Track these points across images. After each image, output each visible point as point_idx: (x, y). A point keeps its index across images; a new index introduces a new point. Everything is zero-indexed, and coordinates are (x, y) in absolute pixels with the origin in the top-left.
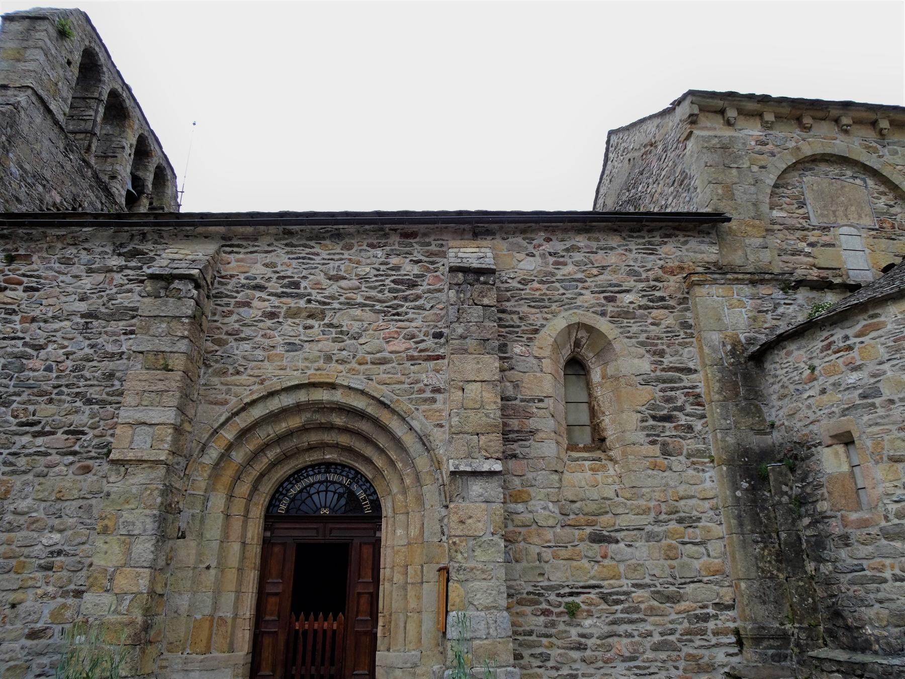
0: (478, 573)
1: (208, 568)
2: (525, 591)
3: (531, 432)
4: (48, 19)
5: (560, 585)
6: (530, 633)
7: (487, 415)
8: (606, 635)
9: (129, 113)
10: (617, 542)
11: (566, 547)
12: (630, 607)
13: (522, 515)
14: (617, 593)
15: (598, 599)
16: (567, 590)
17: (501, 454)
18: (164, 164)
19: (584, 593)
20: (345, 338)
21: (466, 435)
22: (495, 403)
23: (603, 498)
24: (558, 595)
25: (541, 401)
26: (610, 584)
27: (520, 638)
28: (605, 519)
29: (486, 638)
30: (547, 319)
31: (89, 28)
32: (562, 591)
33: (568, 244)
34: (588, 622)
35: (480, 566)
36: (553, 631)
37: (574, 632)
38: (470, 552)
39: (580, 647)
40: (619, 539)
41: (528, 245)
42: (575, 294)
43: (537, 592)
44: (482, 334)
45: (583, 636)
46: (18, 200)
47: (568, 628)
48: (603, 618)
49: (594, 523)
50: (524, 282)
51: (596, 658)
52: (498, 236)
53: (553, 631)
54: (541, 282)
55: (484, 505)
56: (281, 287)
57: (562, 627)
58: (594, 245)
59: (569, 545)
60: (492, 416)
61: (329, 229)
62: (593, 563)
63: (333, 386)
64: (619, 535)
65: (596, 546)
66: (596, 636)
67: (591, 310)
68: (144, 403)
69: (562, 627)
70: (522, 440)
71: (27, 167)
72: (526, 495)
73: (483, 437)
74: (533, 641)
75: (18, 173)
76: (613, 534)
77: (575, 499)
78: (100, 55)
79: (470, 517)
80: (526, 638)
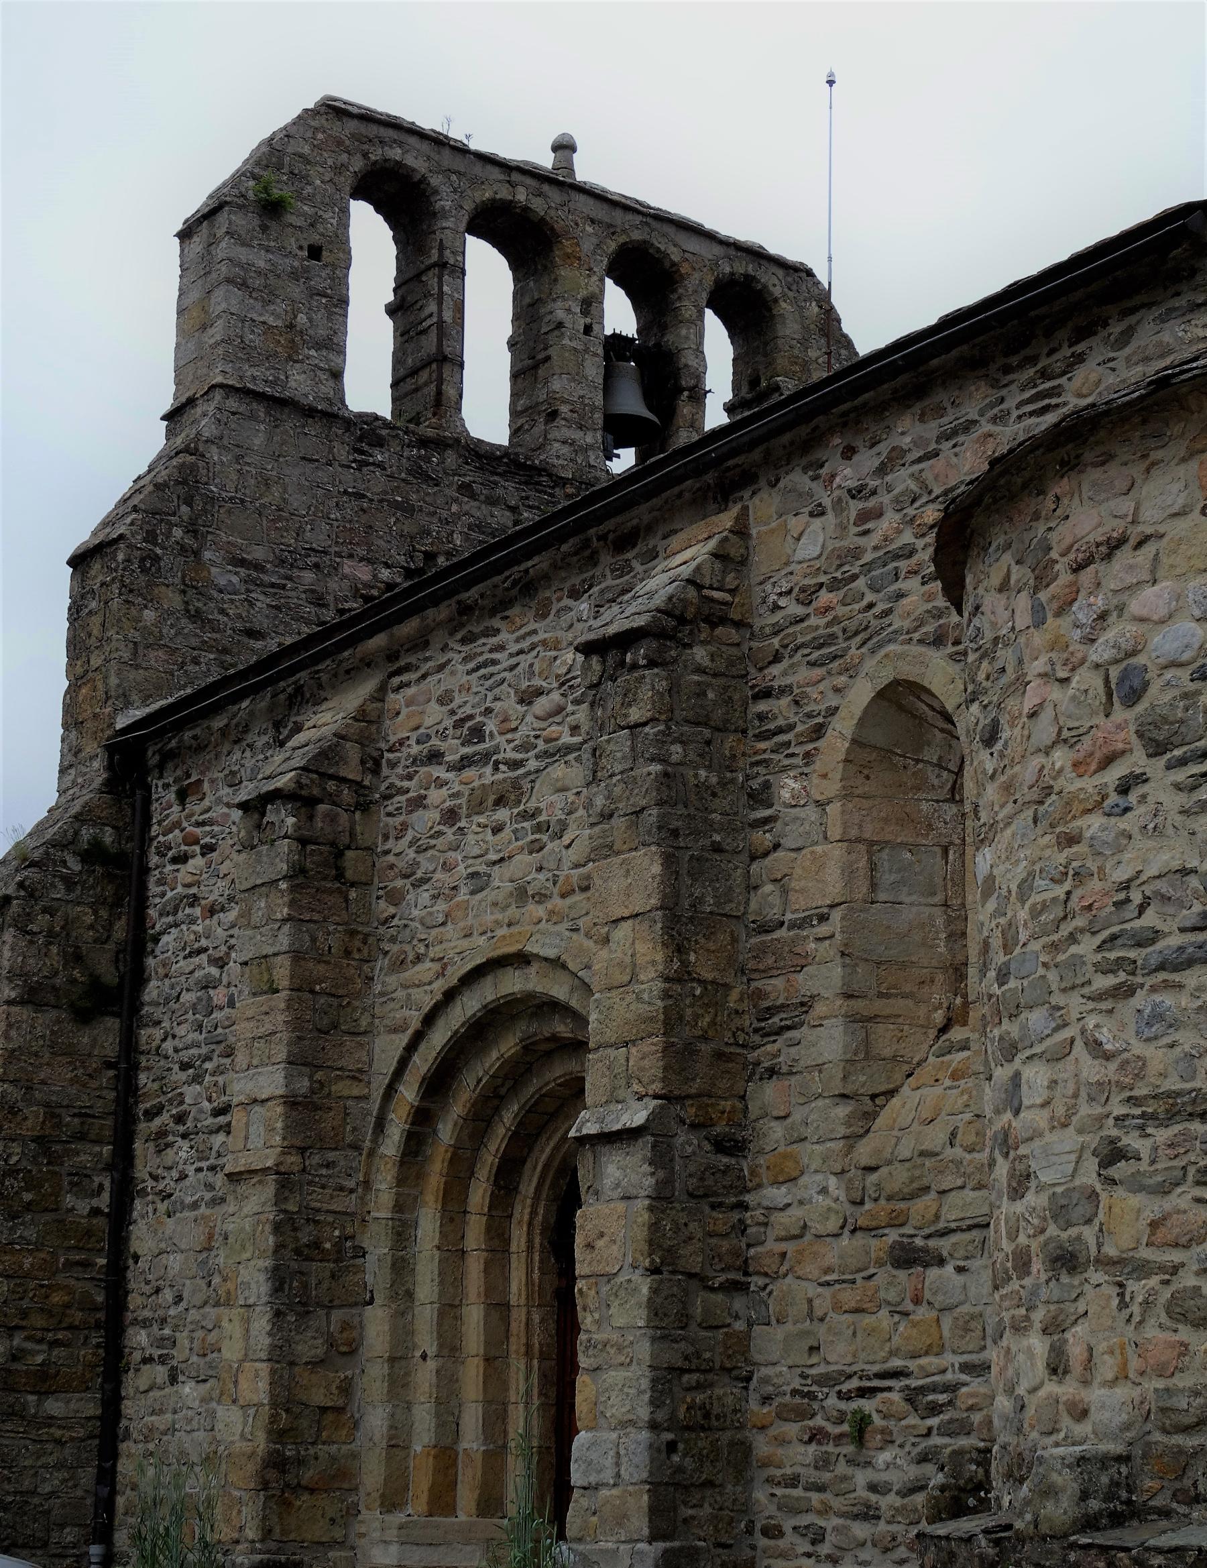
0: (612, 1351)
1: (424, 1357)
2: (788, 1389)
3: (802, 1004)
4: (226, 203)
5: (841, 1373)
6: (793, 1482)
7: (639, 999)
8: (909, 1485)
9: (552, 229)
10: (941, 1262)
11: (853, 1282)
12: (951, 1421)
13: (789, 1212)
14: (934, 1388)
15: (903, 1404)
16: (854, 1383)
17: (660, 1085)
18: (743, 267)
19: (882, 1390)
20: (545, 838)
21: (609, 1050)
22: (654, 963)
23: (922, 1154)
24: (843, 1396)
25: (823, 918)
26: (921, 1368)
27: (779, 1492)
28: (922, 1206)
29: (615, 1485)
30: (837, 690)
31: (352, 125)
32: (845, 1387)
33: (948, 420)
34: (884, 1457)
35: (615, 1337)
36: (827, 1476)
37: (861, 1478)
38: (603, 1308)
39: (868, 1514)
40: (945, 1254)
41: (814, 485)
42: (889, 599)
43: (806, 1389)
44: (632, 801)
45: (873, 1488)
46: (252, 634)
47: (849, 1471)
48: (908, 1448)
49: (900, 1221)
50: (807, 596)
51: (894, 1539)
52: (762, 482)
53: (827, 1476)
54: (834, 585)
55: (621, 1206)
56: (463, 745)
57: (842, 1468)
58: (931, 429)
59: (859, 1276)
60: (646, 996)
61: (517, 576)
62: (897, 1317)
63: (521, 959)
64: (944, 1245)
65: (902, 1275)
66: (895, 1488)
67: (916, 636)
68: (255, 1062)
69: (842, 1468)
70: (789, 1028)
71: (258, 553)
72: (790, 1164)
73: (634, 1050)
74: (798, 1499)
75: (235, 579)
76: (932, 1243)
77: (873, 1163)
78: (410, 161)
79: (602, 1235)
80: (788, 1491)
